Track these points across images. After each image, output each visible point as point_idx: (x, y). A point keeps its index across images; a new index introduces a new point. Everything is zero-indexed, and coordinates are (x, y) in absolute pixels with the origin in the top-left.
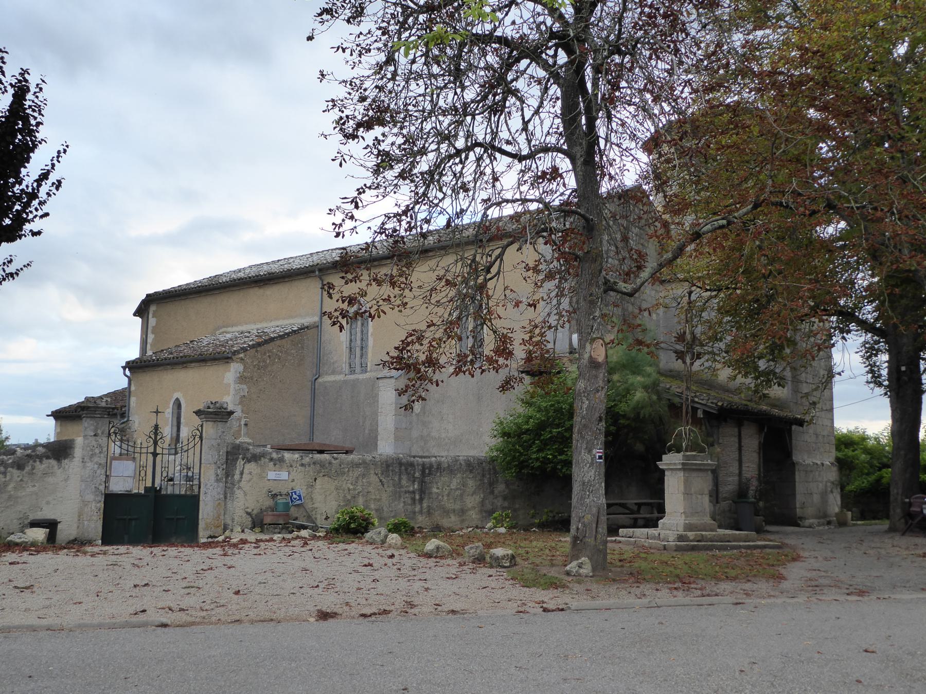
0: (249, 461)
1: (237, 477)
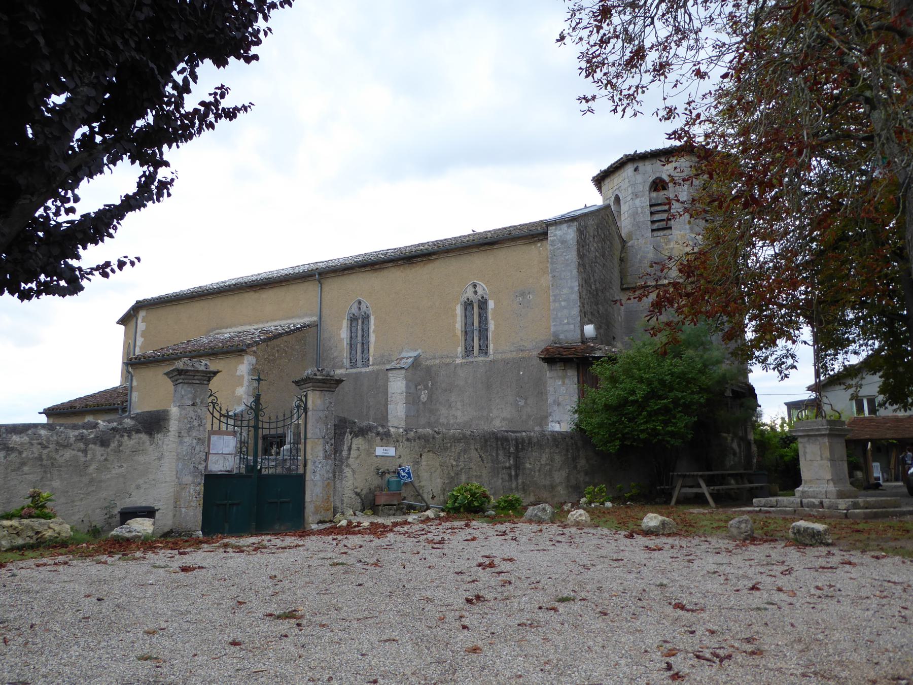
0: (357, 436)
1: (345, 453)
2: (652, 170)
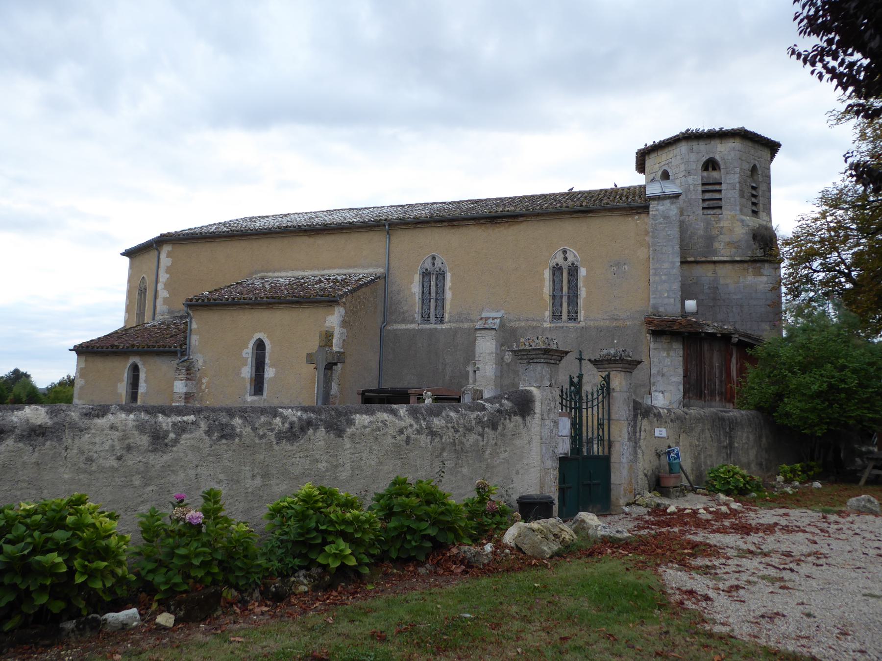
2: (704, 151)
